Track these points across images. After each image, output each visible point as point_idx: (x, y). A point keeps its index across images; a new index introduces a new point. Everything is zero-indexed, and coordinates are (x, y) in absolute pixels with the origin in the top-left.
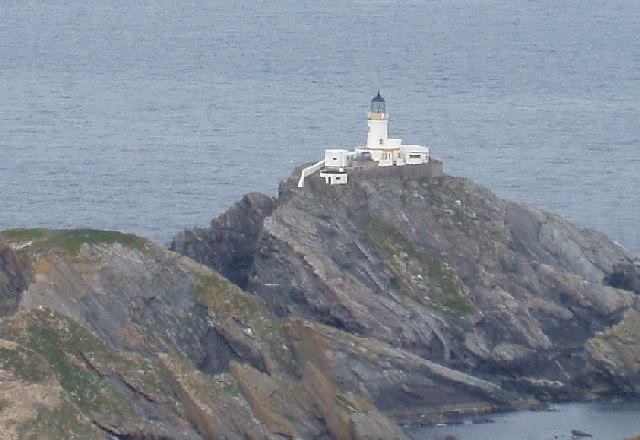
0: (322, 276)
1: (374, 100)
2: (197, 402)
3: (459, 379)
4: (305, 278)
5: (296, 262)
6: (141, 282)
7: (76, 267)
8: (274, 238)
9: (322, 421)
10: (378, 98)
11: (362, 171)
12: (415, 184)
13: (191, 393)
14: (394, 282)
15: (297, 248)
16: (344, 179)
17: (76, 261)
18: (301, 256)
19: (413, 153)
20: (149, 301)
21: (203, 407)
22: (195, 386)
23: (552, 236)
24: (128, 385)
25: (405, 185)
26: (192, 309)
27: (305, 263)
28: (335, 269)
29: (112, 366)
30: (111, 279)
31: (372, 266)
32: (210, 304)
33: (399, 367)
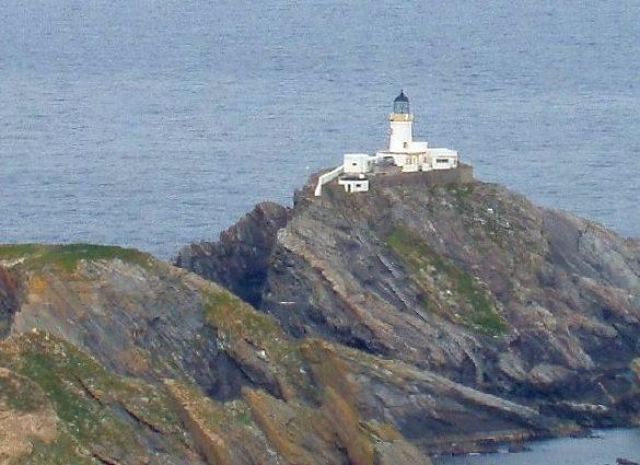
0: (343, 294)
1: (397, 99)
2: (207, 432)
3: (493, 404)
4: (324, 295)
5: (314, 277)
6: (144, 301)
7: (73, 285)
8: (289, 251)
9: (344, 451)
10: (402, 98)
11: (385, 177)
12: (442, 191)
13: (200, 422)
14: (421, 299)
15: (314, 263)
16: (365, 186)
17: (73, 279)
18: (319, 271)
19: (440, 157)
20: (153, 323)
21: (214, 437)
22: (204, 414)
23: (593, 246)
24: (131, 414)
25: (432, 193)
26: (200, 331)
27: (324, 278)
28: (356, 285)
29: (114, 394)
30: (111, 299)
31: (396, 281)
32: (220, 324)
33: (427, 391)
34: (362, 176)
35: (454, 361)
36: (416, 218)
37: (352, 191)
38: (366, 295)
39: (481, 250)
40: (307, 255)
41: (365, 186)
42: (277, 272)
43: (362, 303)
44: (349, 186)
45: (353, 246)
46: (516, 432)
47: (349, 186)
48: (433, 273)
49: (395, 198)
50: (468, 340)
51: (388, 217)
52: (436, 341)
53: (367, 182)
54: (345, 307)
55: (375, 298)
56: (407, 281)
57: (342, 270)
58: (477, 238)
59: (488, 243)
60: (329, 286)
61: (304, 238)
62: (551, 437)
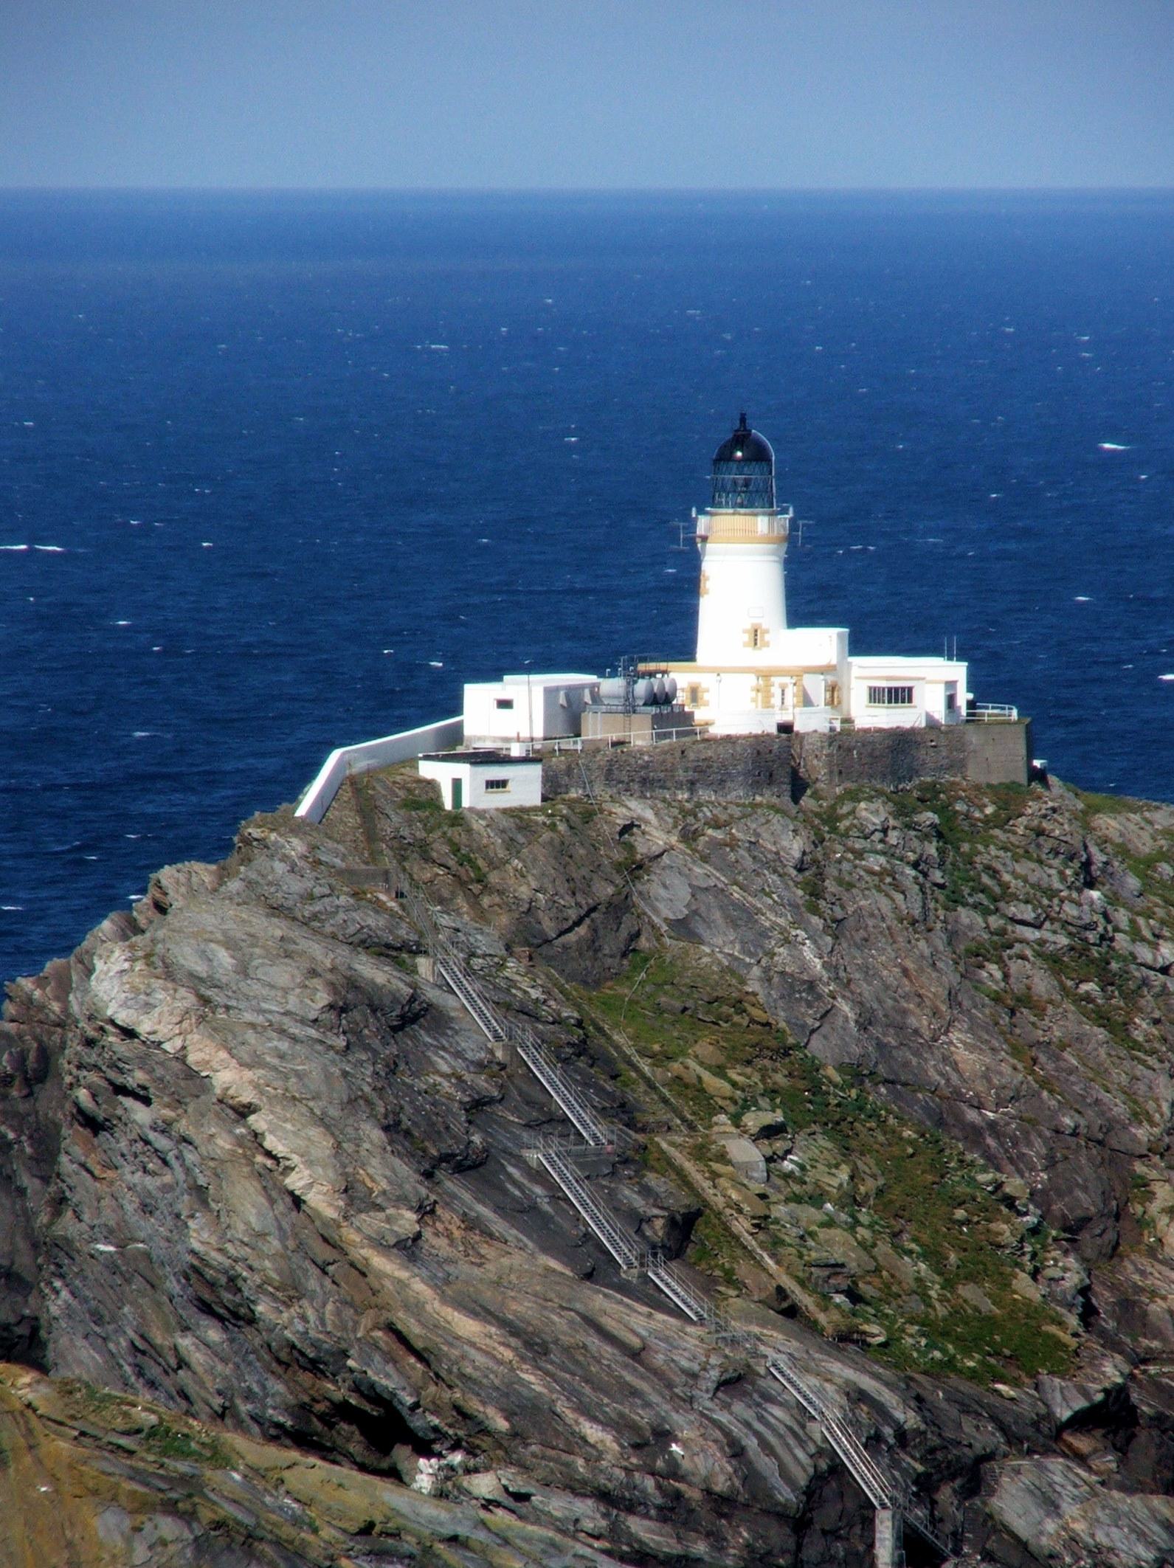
0: (322, 1201)
1: (724, 457)
4: (248, 1206)
8: (129, 1033)
14: (685, 1233)
16: (525, 788)
28: (383, 1169)
34: (516, 751)
35: (776, 1480)
36: (742, 918)
37: (466, 803)
38: (426, 1211)
39: (1024, 1052)
40: (202, 1052)
41: (525, 788)
42: (94, 1125)
43: (409, 1248)
44: (457, 784)
45: (414, 1016)
46: (64, 1341)
47: (457, 784)
48: (770, 1132)
49: (657, 837)
50: (858, 1397)
51: (620, 907)
52: (705, 1401)
53: (536, 771)
54: (329, 1257)
55: (472, 1224)
56: (635, 1161)
57: (334, 1112)
58: (1017, 1002)
59: (1063, 1023)
60: (271, 1171)
61: (195, 981)
62: (497, 809)
